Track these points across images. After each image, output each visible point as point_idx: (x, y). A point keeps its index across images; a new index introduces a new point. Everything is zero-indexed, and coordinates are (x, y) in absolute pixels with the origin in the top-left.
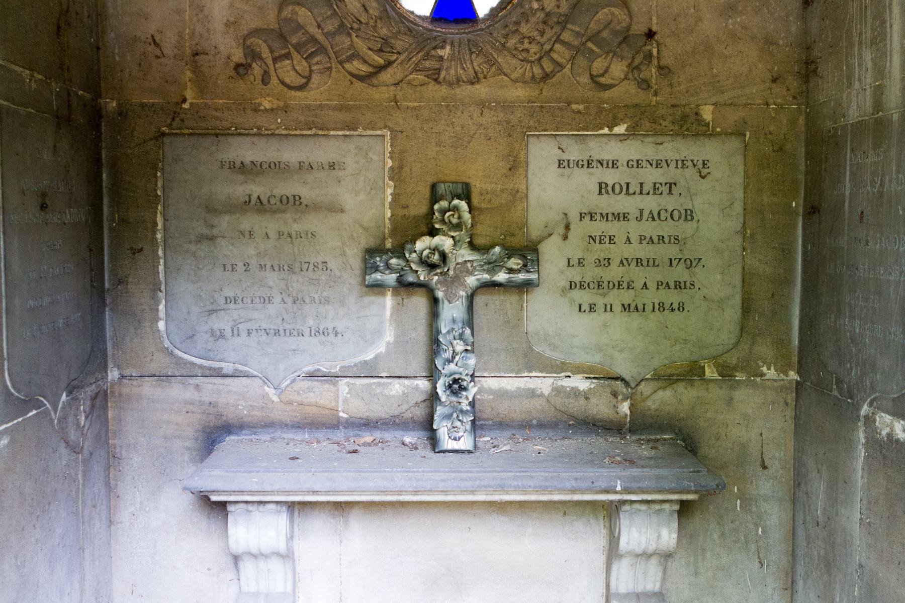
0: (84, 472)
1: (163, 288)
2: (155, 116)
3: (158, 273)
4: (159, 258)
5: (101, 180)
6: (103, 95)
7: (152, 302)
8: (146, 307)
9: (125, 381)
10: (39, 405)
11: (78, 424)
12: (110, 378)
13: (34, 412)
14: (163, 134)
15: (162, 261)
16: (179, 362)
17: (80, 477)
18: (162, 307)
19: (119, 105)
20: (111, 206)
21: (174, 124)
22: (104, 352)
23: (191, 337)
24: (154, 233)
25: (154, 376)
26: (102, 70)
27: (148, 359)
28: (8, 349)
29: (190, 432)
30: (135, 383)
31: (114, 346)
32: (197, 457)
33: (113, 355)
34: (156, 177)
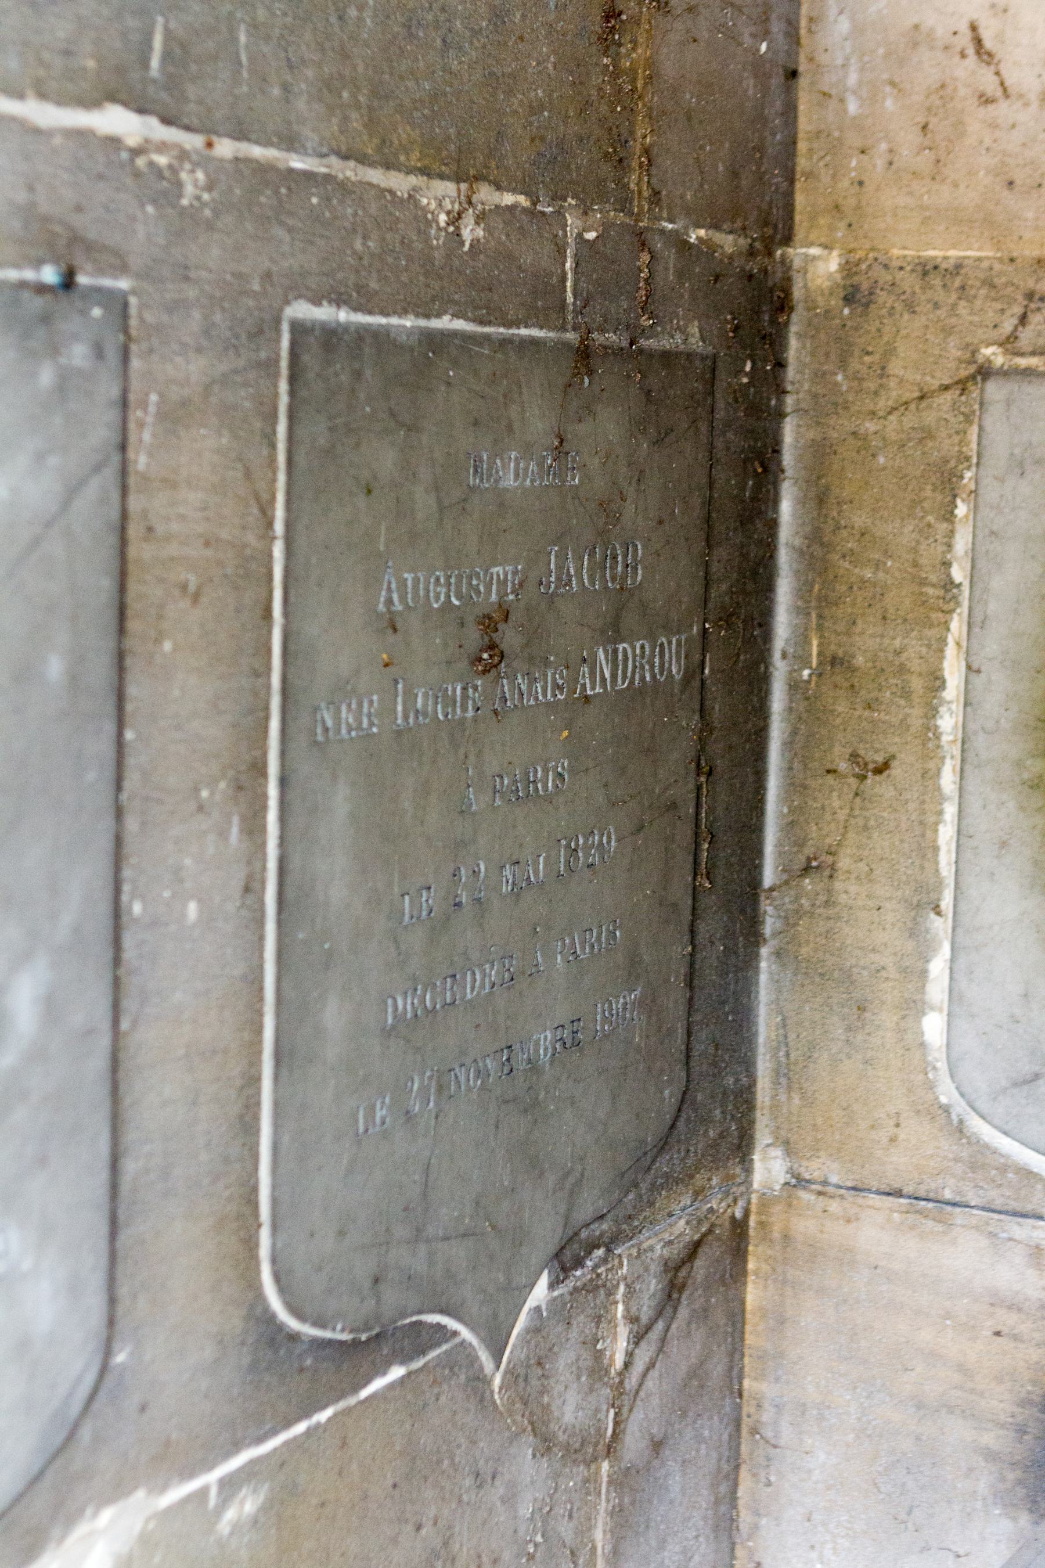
0: (617, 1512)
1: (947, 902)
2: (963, 308)
3: (936, 849)
4: (942, 798)
5: (773, 525)
6: (800, 233)
7: (910, 945)
8: (887, 960)
9: (803, 1195)
10: (420, 1339)
11: (598, 1368)
12: (758, 1178)
13: (397, 1372)
14: (985, 372)
15: (950, 810)
16: (981, 1160)
17: (599, 1535)
18: (938, 967)
19: (849, 268)
20: (801, 611)
21: (1027, 337)
22: (743, 1101)
23: (1026, 1082)
24: (932, 712)
25: (898, 1193)
26: (802, 146)
27: (883, 1135)
28: (274, 1187)
29: (1000, 1402)
30: (834, 1206)
31: (777, 1072)
32: (1021, 1492)
33: (775, 1107)
34: (949, 516)
